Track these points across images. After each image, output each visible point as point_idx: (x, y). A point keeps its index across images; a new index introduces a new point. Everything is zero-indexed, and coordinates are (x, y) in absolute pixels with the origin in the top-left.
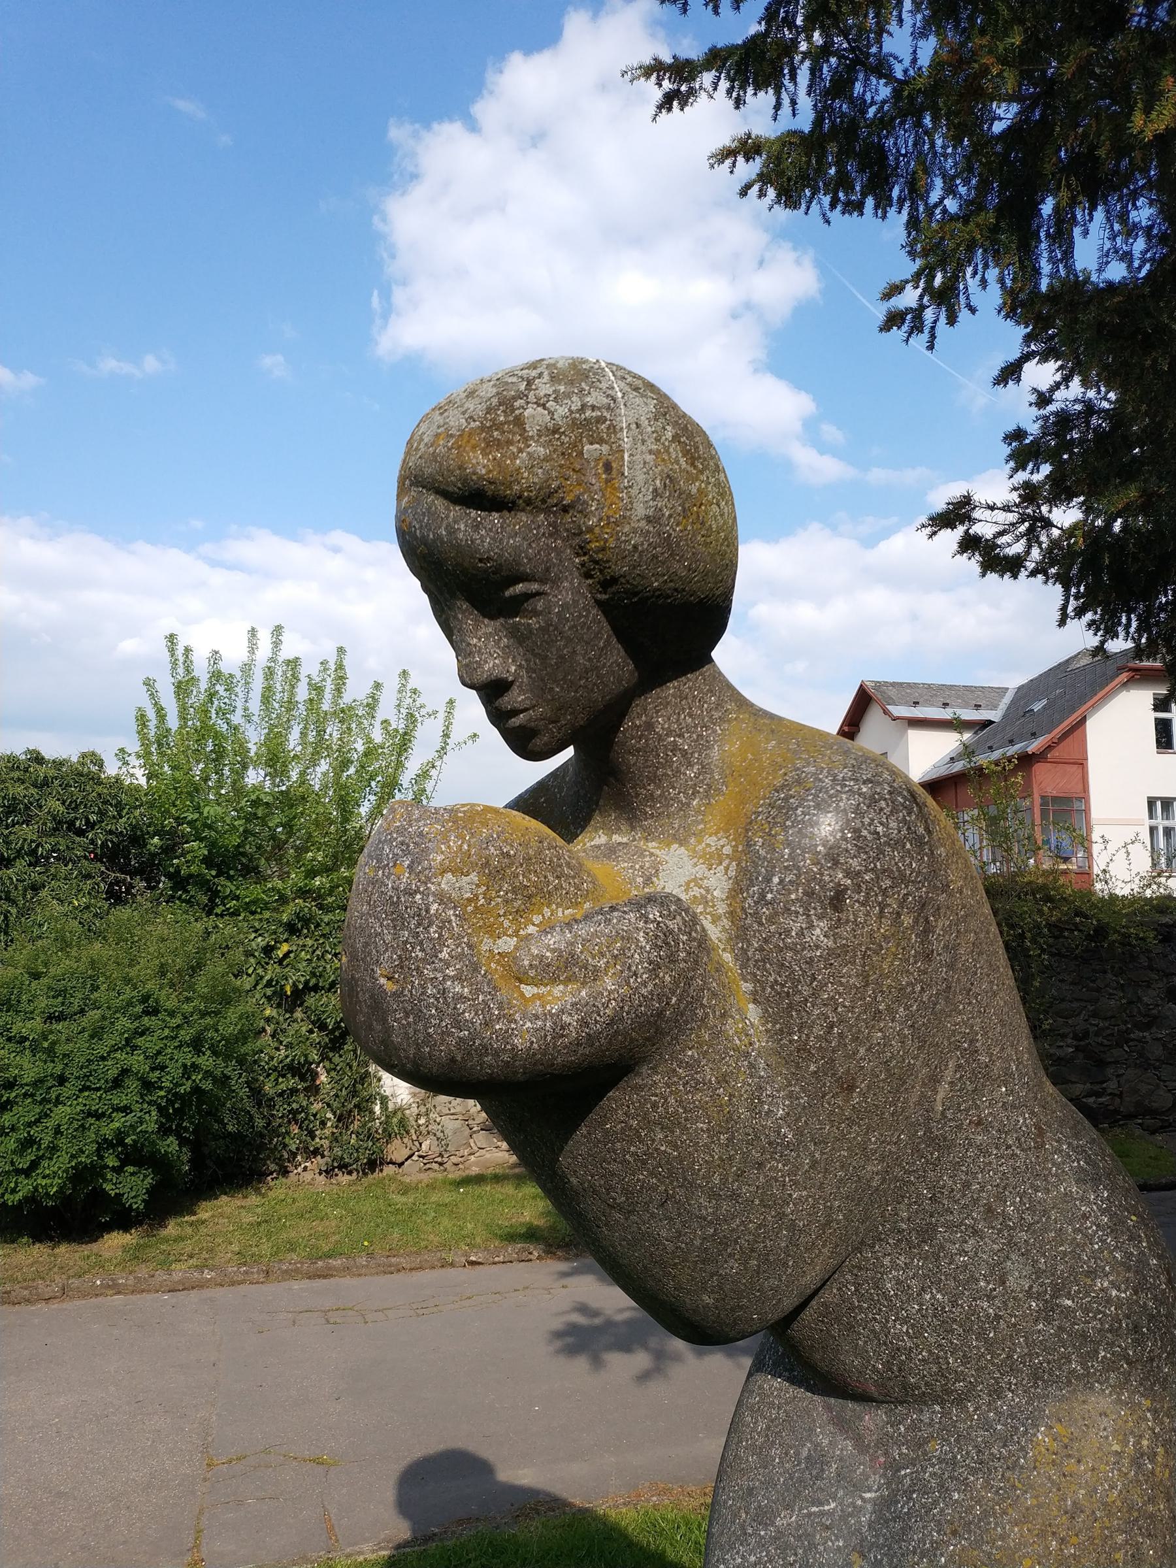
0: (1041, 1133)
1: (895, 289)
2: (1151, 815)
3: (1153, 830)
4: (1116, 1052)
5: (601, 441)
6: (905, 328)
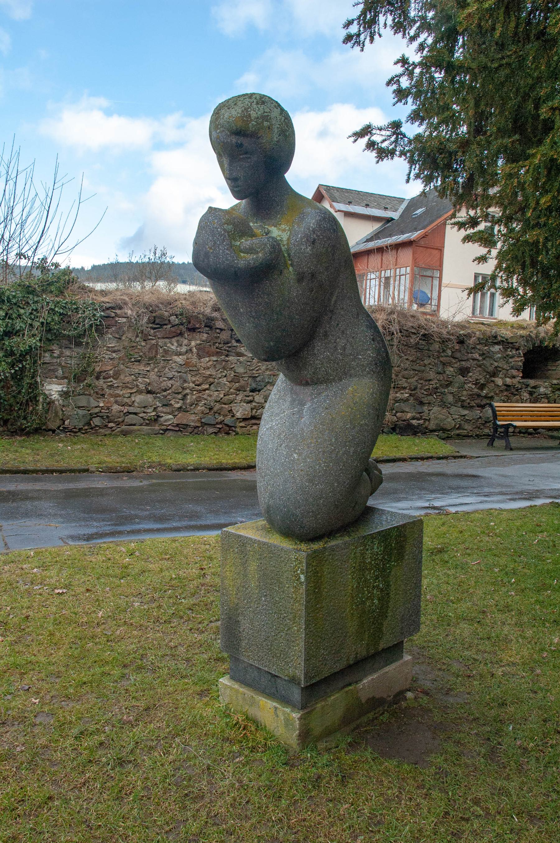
0: (358, 314)
1: (349, 23)
4: (430, 398)
6: (352, 42)
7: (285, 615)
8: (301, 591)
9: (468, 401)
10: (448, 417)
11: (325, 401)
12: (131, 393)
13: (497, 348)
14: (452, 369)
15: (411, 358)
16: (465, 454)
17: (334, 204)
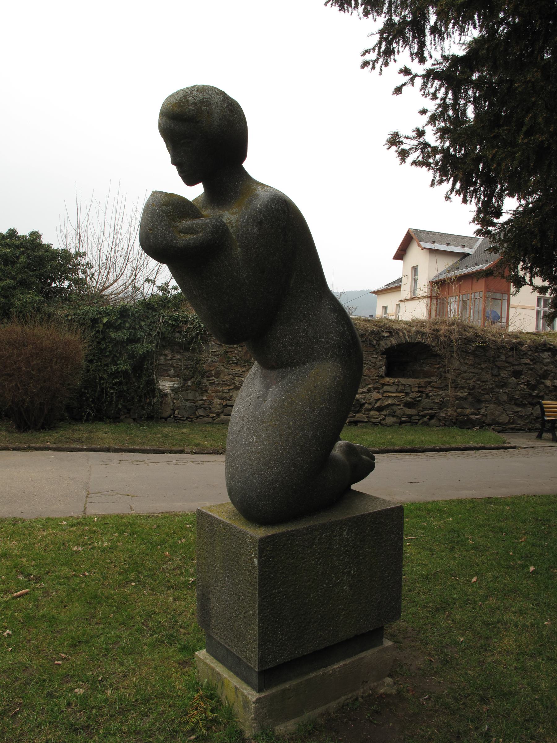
2: (538, 305)
3: (538, 312)
4: (487, 396)
5: (207, 106)
7: (243, 597)
8: (255, 575)
9: (521, 399)
10: (503, 413)
11: (287, 384)
12: (229, 390)
13: (546, 354)
14: (506, 372)
15: (469, 363)
16: (513, 444)
17: (421, 243)
